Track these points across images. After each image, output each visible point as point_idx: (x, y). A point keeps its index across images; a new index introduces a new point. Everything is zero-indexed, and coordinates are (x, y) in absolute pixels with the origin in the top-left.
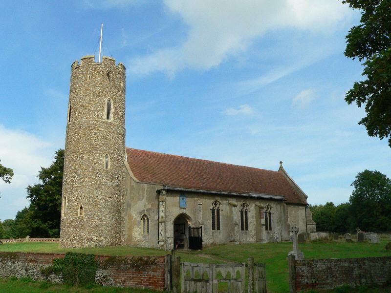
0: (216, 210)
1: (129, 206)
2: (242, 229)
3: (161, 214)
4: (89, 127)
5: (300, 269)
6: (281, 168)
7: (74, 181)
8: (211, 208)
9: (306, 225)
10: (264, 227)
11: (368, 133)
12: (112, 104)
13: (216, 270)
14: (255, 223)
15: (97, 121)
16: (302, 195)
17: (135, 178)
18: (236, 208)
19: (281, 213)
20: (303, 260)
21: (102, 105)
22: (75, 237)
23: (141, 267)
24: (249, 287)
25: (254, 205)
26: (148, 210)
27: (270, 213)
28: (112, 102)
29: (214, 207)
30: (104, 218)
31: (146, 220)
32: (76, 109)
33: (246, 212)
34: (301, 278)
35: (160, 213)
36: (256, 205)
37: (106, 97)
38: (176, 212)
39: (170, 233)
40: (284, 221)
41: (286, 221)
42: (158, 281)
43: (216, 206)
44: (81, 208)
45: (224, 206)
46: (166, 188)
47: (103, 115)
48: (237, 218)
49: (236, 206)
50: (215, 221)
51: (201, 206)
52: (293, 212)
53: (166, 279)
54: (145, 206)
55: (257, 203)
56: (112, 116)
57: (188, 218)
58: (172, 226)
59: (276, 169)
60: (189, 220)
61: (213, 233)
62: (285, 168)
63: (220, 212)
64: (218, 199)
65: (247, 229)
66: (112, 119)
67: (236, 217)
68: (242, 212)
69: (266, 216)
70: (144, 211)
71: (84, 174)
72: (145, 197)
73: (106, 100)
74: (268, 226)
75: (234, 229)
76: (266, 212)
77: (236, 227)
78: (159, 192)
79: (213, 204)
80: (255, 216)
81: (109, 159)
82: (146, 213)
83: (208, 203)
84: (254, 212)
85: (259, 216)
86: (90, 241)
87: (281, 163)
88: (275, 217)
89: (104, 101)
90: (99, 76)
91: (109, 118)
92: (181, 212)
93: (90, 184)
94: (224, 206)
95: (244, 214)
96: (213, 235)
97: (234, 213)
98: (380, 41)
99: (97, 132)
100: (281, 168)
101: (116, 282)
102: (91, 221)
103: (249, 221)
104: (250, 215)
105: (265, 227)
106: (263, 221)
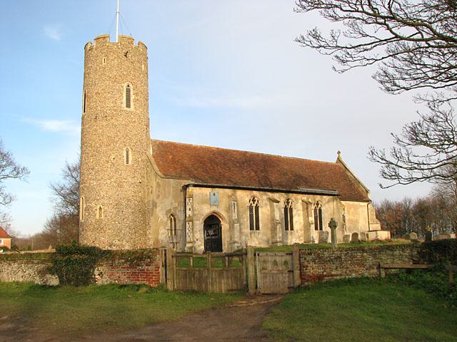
3: (188, 213)
5: (305, 259)
6: (339, 160)
10: (313, 226)
12: (132, 90)
15: (115, 111)
21: (119, 91)
28: (131, 85)
30: (125, 220)
49: (278, 202)
57: (221, 217)
59: (333, 160)
81: (130, 152)
87: (339, 153)
91: (128, 106)
100: (339, 160)
106: (312, 219)
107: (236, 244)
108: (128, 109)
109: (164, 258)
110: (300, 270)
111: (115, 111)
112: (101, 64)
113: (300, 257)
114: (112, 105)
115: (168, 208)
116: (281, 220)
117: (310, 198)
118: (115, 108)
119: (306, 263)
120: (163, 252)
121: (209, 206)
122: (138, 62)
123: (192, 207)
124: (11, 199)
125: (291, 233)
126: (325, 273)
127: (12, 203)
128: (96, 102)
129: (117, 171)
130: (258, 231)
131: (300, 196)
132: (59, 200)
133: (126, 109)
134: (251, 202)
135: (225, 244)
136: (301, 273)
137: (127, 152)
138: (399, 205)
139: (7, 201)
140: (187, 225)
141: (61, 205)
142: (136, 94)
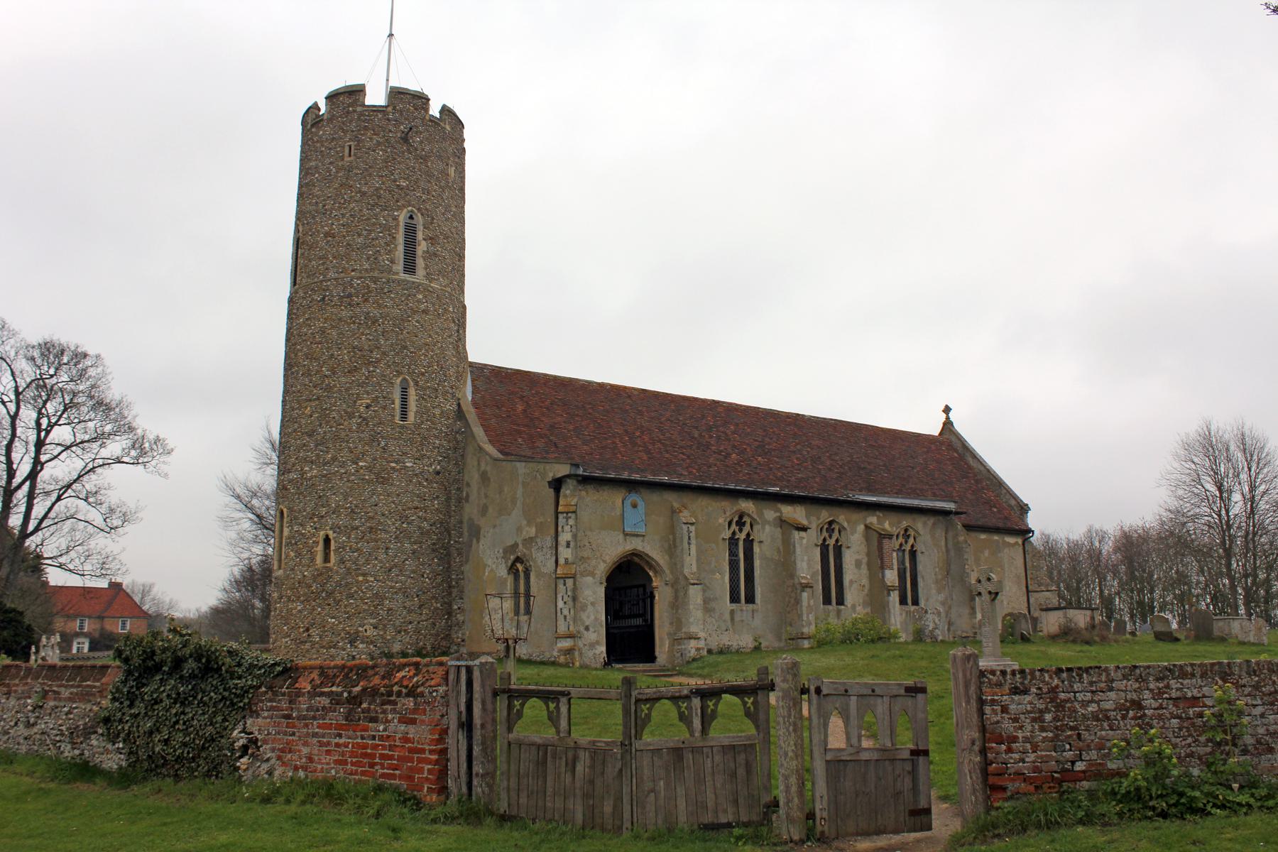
0: (741, 544)
1: (476, 532)
2: (827, 601)
3: (565, 553)
4: (350, 296)
5: (1005, 709)
6: (948, 425)
7: (306, 460)
8: (727, 534)
9: (1028, 591)
10: (895, 596)
12: (420, 228)
14: (865, 581)
15: (375, 280)
16: (1013, 502)
17: (489, 448)
18: (803, 534)
19: (948, 551)
20: (1013, 673)
21: (389, 230)
22: (308, 630)
23: (365, 705)
24: (175, 819)
25: (861, 528)
26: (529, 541)
27: (913, 553)
28: (419, 219)
29: (734, 533)
30: (395, 572)
31: (522, 575)
32: (311, 248)
33: (838, 550)
34: (1009, 750)
35: (561, 549)
36: (867, 527)
37: (400, 209)
38: (612, 549)
39: (595, 614)
40: (952, 572)
41: (963, 577)
42: (420, 761)
43: (741, 530)
44: (327, 540)
45: (767, 527)
46: (580, 471)
47: (392, 262)
48: (807, 565)
49: (804, 529)
50: (738, 575)
51: (692, 528)
52: (987, 553)
53: (452, 754)
54: (519, 529)
55: (873, 519)
56: (420, 263)
57: (651, 567)
58: (601, 592)
59: (931, 426)
60: (656, 572)
61: (732, 612)
62: (959, 427)
63: (756, 549)
64: (747, 506)
65: (840, 601)
66: (421, 272)
67: (805, 565)
68: (824, 548)
69: (902, 562)
70: (516, 545)
71: (336, 438)
72: (519, 504)
73: (403, 217)
74: (909, 594)
75: (798, 601)
76: (901, 549)
77: (805, 595)
78: (557, 484)
79: (730, 524)
80: (865, 560)
81: (412, 392)
82: (521, 551)
83: (719, 513)
84: (864, 549)
85: (877, 562)
86: (352, 642)
87: (947, 410)
88: (928, 566)
89: (395, 219)
91: (410, 267)
93: (352, 468)
94: (767, 527)
95: (831, 557)
96: (732, 619)
97: (798, 551)
99: (375, 312)
100: (948, 425)
101: (284, 764)
102: (357, 582)
103: (847, 578)
104: (849, 558)
105: (897, 593)
106: (891, 577)
107: (693, 643)
108: (408, 277)
109: (463, 699)
110: (983, 751)
111: (375, 280)
112: (342, 158)
113: (982, 702)
114: (367, 266)
115: (510, 542)
116: (813, 575)
117: (888, 524)
118: (376, 274)
119: (1007, 726)
120: (463, 671)
121: (621, 536)
122: (440, 157)
123: (575, 536)
124: (125, 519)
125: (839, 612)
126: (1080, 766)
127: (128, 528)
128: (324, 257)
129: (373, 439)
130: (751, 606)
131: (856, 516)
132: (246, 523)
133: (402, 276)
134: (734, 526)
135: (661, 639)
136: (987, 763)
137: (404, 391)
138: (1074, 548)
139: (116, 522)
140: (561, 586)
141: (250, 536)
142: (431, 240)
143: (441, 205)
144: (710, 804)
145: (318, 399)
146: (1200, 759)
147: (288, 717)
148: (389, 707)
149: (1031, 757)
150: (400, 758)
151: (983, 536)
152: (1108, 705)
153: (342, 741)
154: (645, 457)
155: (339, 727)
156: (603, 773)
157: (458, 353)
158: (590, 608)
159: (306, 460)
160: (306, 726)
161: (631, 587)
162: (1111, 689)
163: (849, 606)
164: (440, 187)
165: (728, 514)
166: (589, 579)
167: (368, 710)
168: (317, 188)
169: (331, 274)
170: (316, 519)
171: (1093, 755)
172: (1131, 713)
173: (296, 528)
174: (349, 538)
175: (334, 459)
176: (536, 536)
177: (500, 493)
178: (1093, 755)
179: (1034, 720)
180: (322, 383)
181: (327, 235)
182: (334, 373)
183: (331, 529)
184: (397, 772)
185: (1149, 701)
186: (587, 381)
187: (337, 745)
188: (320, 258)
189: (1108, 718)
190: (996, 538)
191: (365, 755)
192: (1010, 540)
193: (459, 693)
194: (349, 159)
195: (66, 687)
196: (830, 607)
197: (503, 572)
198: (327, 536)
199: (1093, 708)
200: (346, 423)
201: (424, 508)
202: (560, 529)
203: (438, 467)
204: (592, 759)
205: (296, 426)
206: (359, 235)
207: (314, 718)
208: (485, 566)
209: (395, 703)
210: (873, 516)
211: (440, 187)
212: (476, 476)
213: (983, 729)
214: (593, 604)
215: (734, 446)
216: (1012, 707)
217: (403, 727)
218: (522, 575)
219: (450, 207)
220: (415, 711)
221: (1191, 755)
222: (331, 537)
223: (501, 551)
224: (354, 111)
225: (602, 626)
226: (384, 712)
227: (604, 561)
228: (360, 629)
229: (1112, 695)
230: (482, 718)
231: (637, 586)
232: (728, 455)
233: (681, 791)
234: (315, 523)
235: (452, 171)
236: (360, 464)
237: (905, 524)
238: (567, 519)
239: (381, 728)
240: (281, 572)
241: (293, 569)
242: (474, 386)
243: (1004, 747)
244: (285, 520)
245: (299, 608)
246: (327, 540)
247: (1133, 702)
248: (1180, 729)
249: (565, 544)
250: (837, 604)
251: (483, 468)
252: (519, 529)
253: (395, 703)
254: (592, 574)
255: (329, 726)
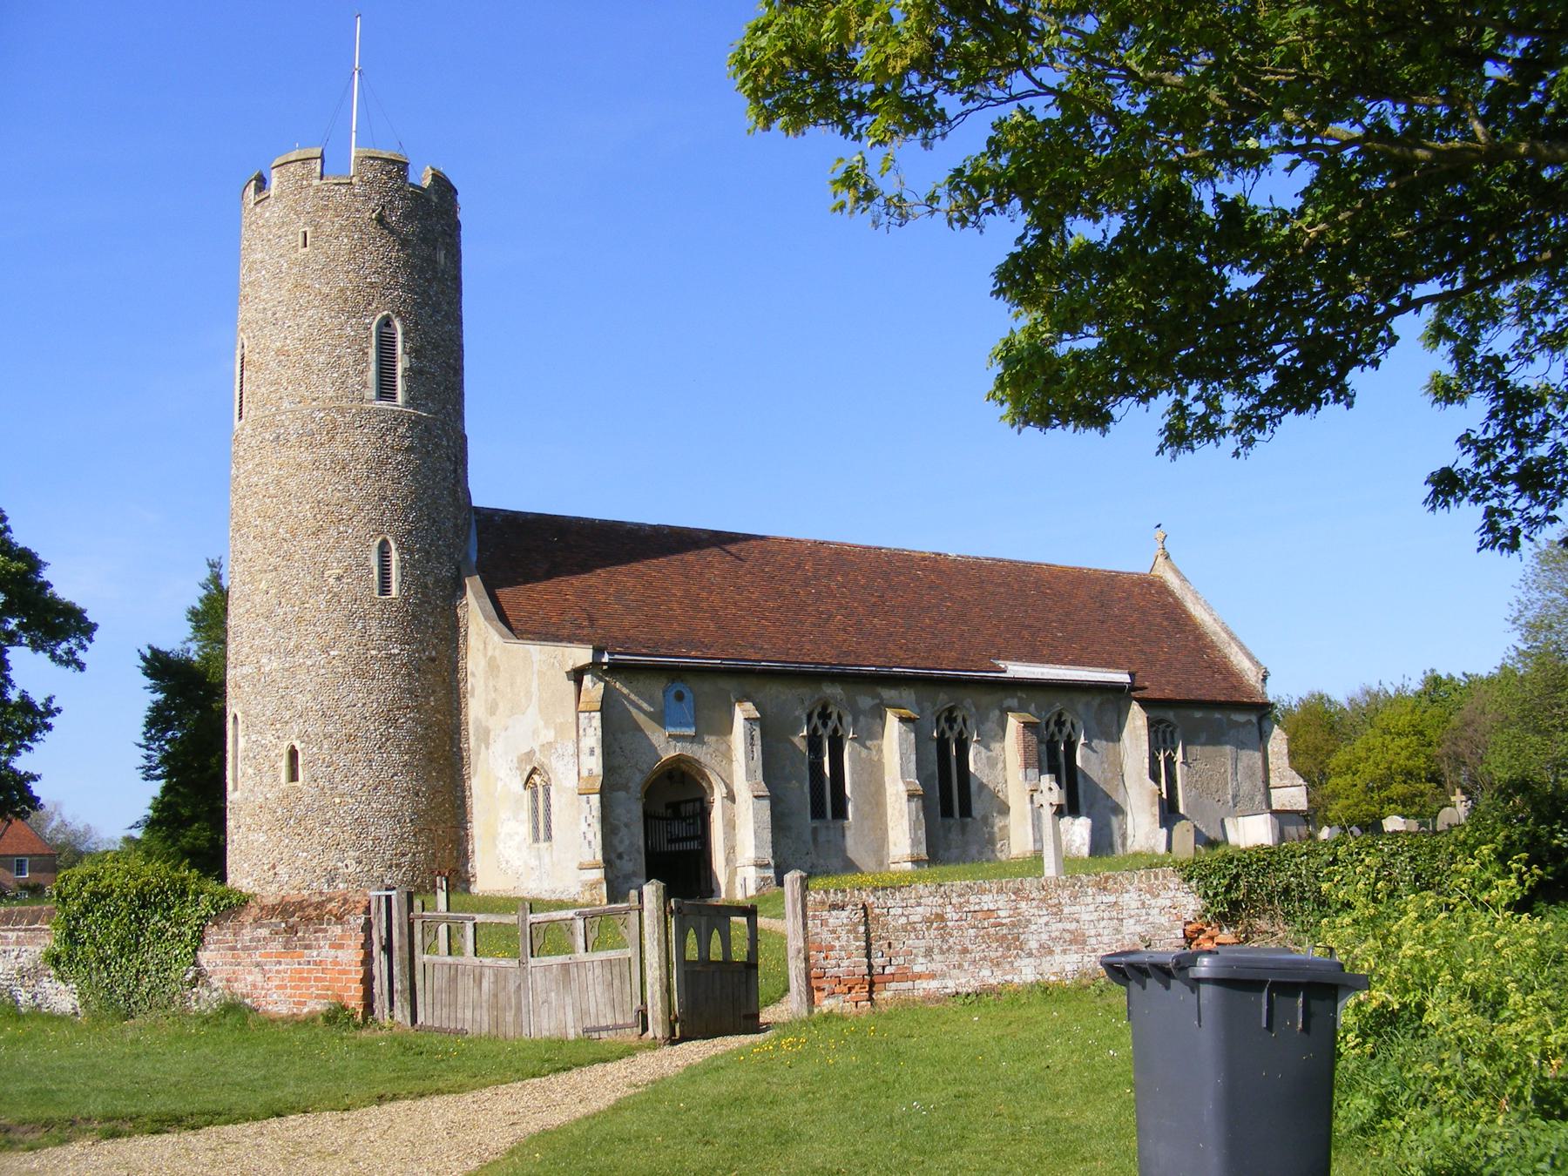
11: (1301, 410)
13: (371, 401)
22: (274, 867)
31: (540, 789)
42: (348, 981)
44: (293, 754)
50: (824, 804)
54: (535, 732)
58: (637, 810)
61: (815, 831)
64: (833, 691)
70: (531, 754)
72: (535, 699)
79: (938, 720)
82: (539, 758)
90: (342, 228)
92: (481, 619)
96: (815, 840)
98: (1234, 127)
108: (384, 404)
110: (807, 959)
118: (344, 403)
119: (826, 936)
120: (383, 899)
134: (815, 719)
143: (427, 304)
144: (593, 1010)
145: (276, 569)
146: (992, 961)
147: (233, 948)
148: (321, 935)
149: (845, 963)
150: (332, 980)
151: (1198, 715)
152: (913, 918)
153: (281, 968)
154: (712, 627)
155: (280, 955)
156: (505, 988)
157: (456, 499)
158: (624, 831)
159: (263, 650)
160: (250, 955)
161: (687, 802)
162: (919, 905)
163: (979, 817)
164: (427, 280)
165: (807, 703)
166: (622, 794)
167: (303, 938)
168: (264, 290)
169: (286, 405)
170: (278, 726)
171: (901, 960)
172: (935, 925)
173: (253, 738)
174: (320, 748)
175: (298, 647)
176: (556, 741)
177: (512, 685)
178: (901, 960)
179: (849, 932)
180: (280, 548)
181: (279, 352)
182: (294, 536)
183: (298, 738)
184: (330, 993)
185: (950, 913)
186: (637, 524)
187: (278, 972)
188: (271, 384)
189: (915, 929)
190: (1217, 715)
191: (302, 979)
192: (1240, 718)
193: (380, 920)
194: (304, 250)
195: (13, 930)
196: (952, 821)
197: (517, 784)
198: (293, 747)
199: (903, 920)
200: (311, 601)
201: (416, 707)
202: (581, 732)
203: (434, 653)
204: (496, 976)
205: (249, 605)
206: (321, 352)
207: (256, 948)
208: (498, 779)
209: (325, 931)
210: (1012, 697)
211: (427, 280)
212: (483, 663)
213: (806, 940)
214: (626, 825)
215: (840, 606)
216: (831, 920)
217: (333, 952)
218: (540, 789)
219: (440, 304)
220: (342, 938)
221: (984, 959)
222: (297, 748)
223: (515, 760)
224: (310, 185)
225: (639, 853)
226: (317, 939)
227: (641, 771)
228: (340, 864)
229: (919, 909)
230: (400, 941)
231: (694, 800)
232: (831, 616)
233: (569, 1000)
234: (277, 730)
235: (441, 256)
236: (332, 653)
237: (1058, 706)
238: (590, 719)
239: (315, 953)
240: (238, 794)
241: (251, 791)
242: (480, 542)
243: (823, 955)
244: (240, 727)
245: (262, 839)
246: (293, 754)
247: (937, 915)
248: (976, 937)
249: (588, 751)
250: (961, 816)
251: (490, 654)
252: (535, 732)
253: (325, 931)
254: (626, 788)
255: (270, 955)
